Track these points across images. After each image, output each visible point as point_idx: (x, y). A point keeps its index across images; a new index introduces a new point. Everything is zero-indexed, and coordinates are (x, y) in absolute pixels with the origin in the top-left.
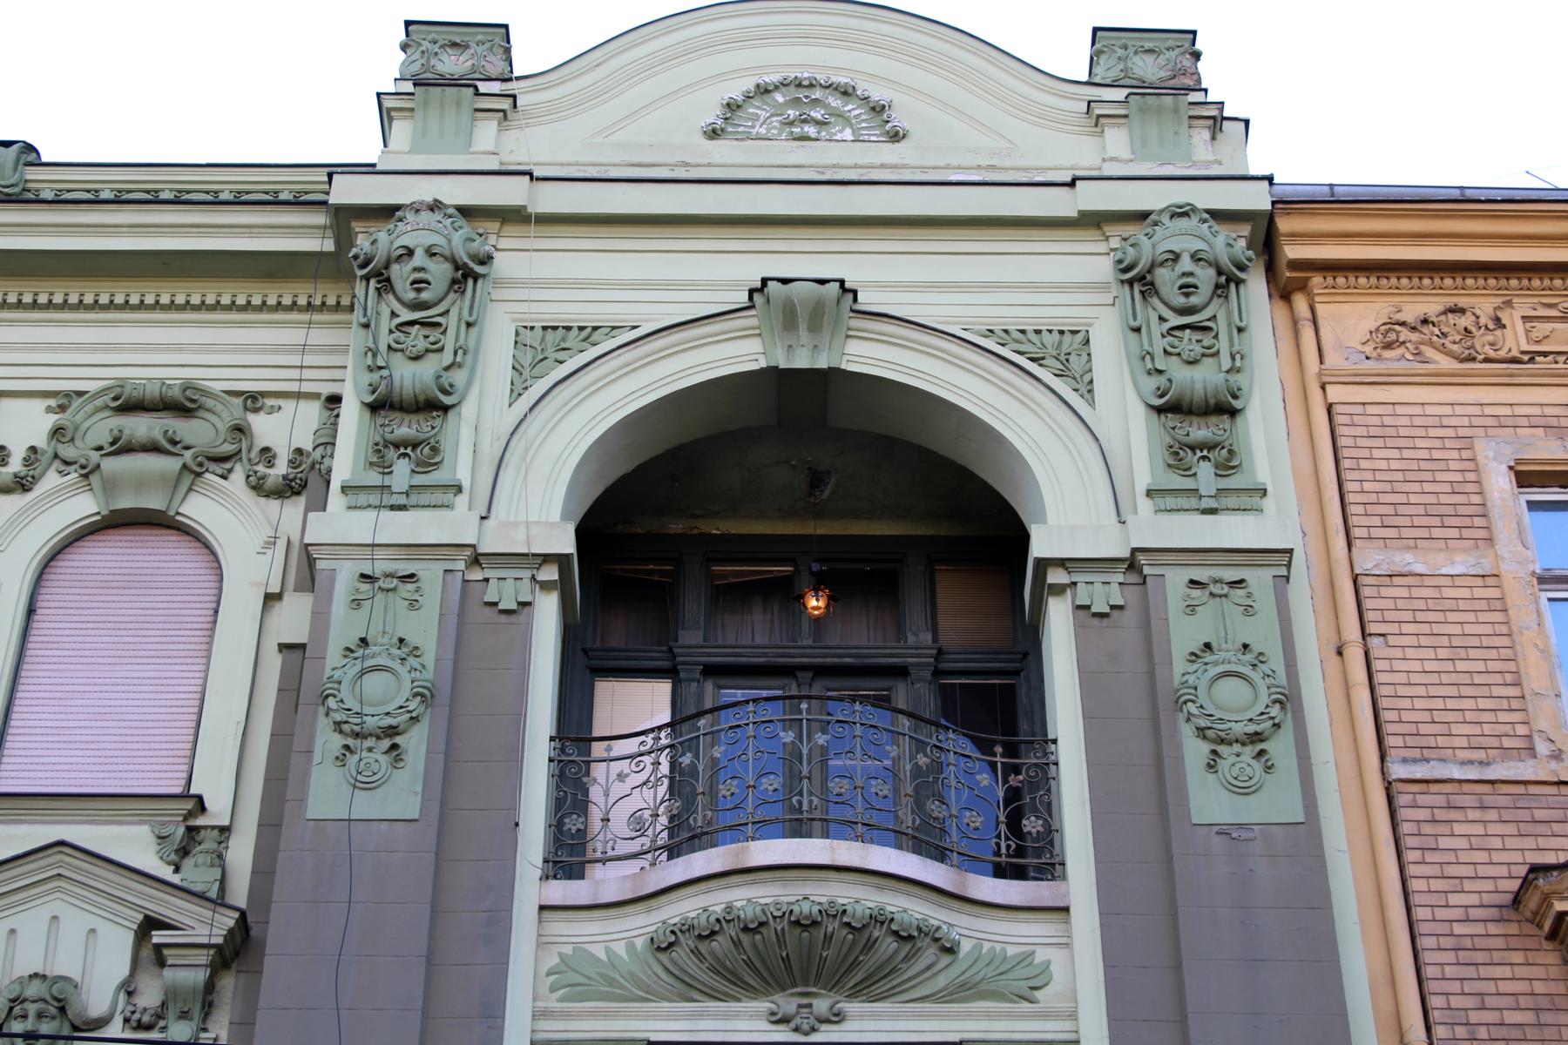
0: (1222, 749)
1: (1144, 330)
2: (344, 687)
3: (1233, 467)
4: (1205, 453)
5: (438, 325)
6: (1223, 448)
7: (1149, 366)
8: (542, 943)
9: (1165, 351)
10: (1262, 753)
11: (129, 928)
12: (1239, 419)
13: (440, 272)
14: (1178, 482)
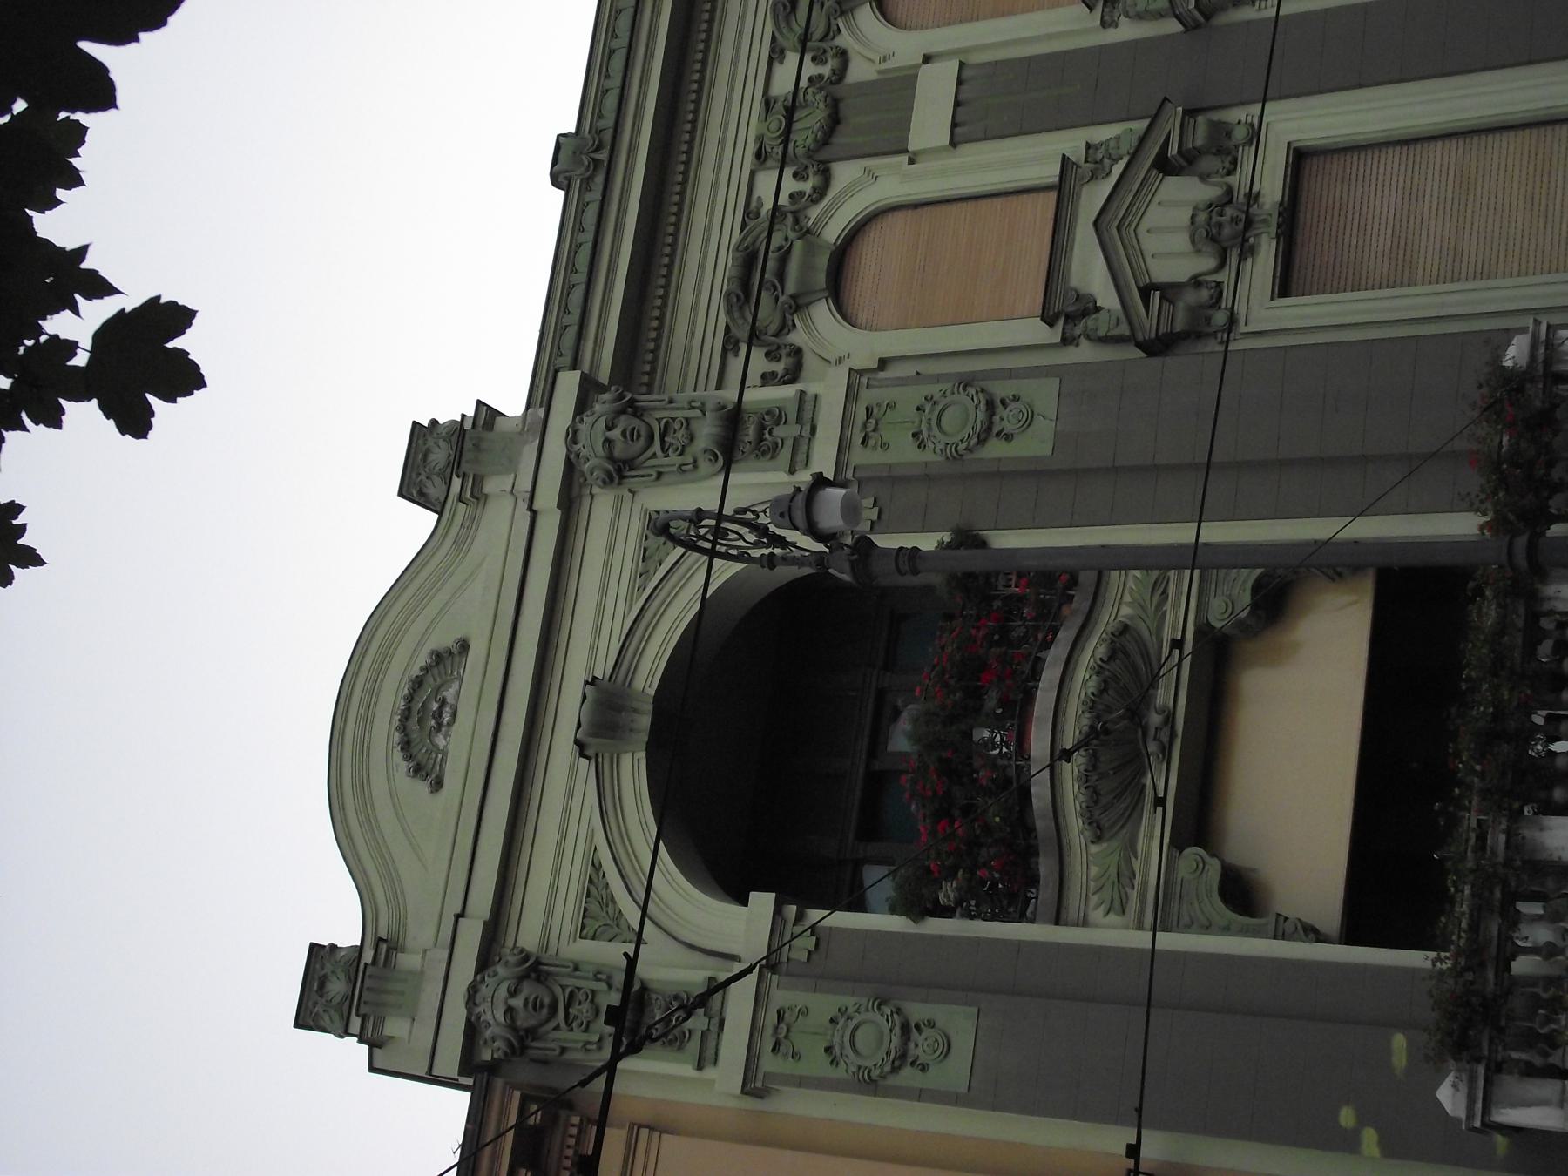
0: (996, 429)
1: (661, 470)
2: (950, 442)
3: (780, 413)
4: (767, 432)
5: (572, 993)
6: (764, 419)
7: (594, 1047)
8: (1084, 922)
9: (680, 455)
10: (917, 1027)
11: (1161, 180)
12: (651, 986)
13: (528, 989)
14: (785, 454)
